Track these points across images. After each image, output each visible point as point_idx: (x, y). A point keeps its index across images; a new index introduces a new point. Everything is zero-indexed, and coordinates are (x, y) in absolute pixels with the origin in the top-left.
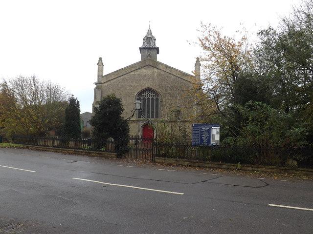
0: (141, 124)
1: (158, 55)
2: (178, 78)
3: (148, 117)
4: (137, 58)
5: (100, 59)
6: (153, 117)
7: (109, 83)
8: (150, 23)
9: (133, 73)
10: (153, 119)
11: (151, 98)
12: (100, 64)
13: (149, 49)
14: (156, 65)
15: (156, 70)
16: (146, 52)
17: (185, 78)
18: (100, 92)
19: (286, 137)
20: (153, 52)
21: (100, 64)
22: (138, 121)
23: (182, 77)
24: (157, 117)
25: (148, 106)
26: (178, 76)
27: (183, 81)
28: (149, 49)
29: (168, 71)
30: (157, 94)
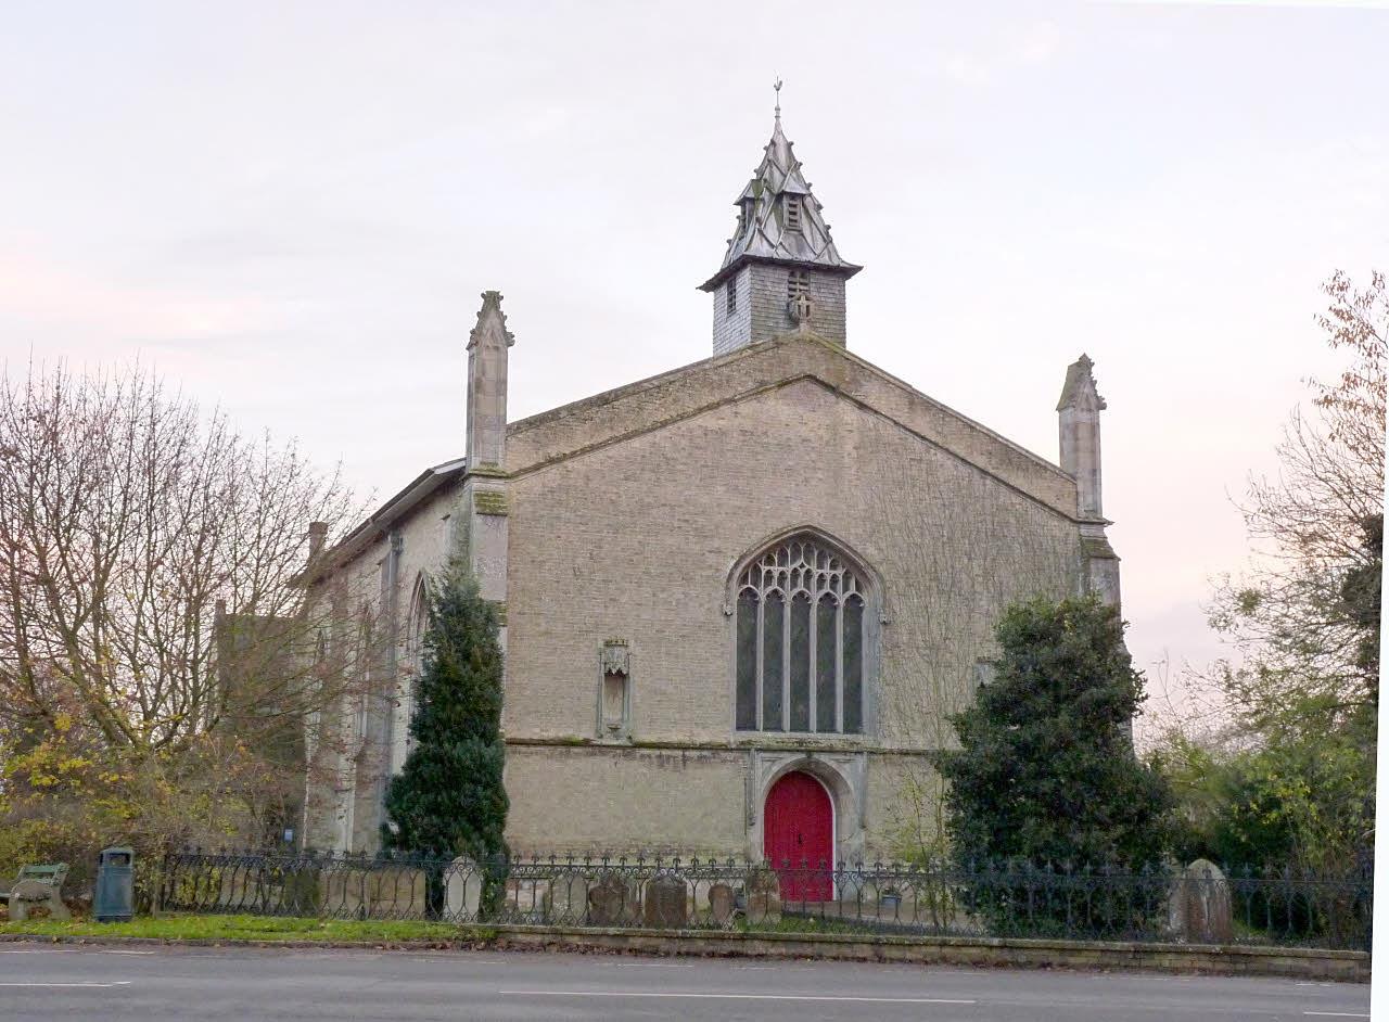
0: (765, 772)
1: (510, 349)
2: (976, 475)
3: (800, 724)
4: (686, 332)
5: (492, 300)
6: (827, 725)
7: (552, 475)
8: (784, 97)
9: (708, 421)
10: (826, 739)
11: (815, 596)
12: (490, 336)
13: (784, 266)
14: (847, 380)
15: (848, 413)
16: (784, 289)
17: (1018, 481)
18: (504, 539)
19: (228, 711)
20: (817, 289)
21: (490, 336)
22: (744, 748)
23: (1003, 476)
24: (853, 724)
25: (800, 648)
26: (981, 462)
27: (1006, 497)
28: (784, 266)
29: (922, 424)
30: (854, 569)
